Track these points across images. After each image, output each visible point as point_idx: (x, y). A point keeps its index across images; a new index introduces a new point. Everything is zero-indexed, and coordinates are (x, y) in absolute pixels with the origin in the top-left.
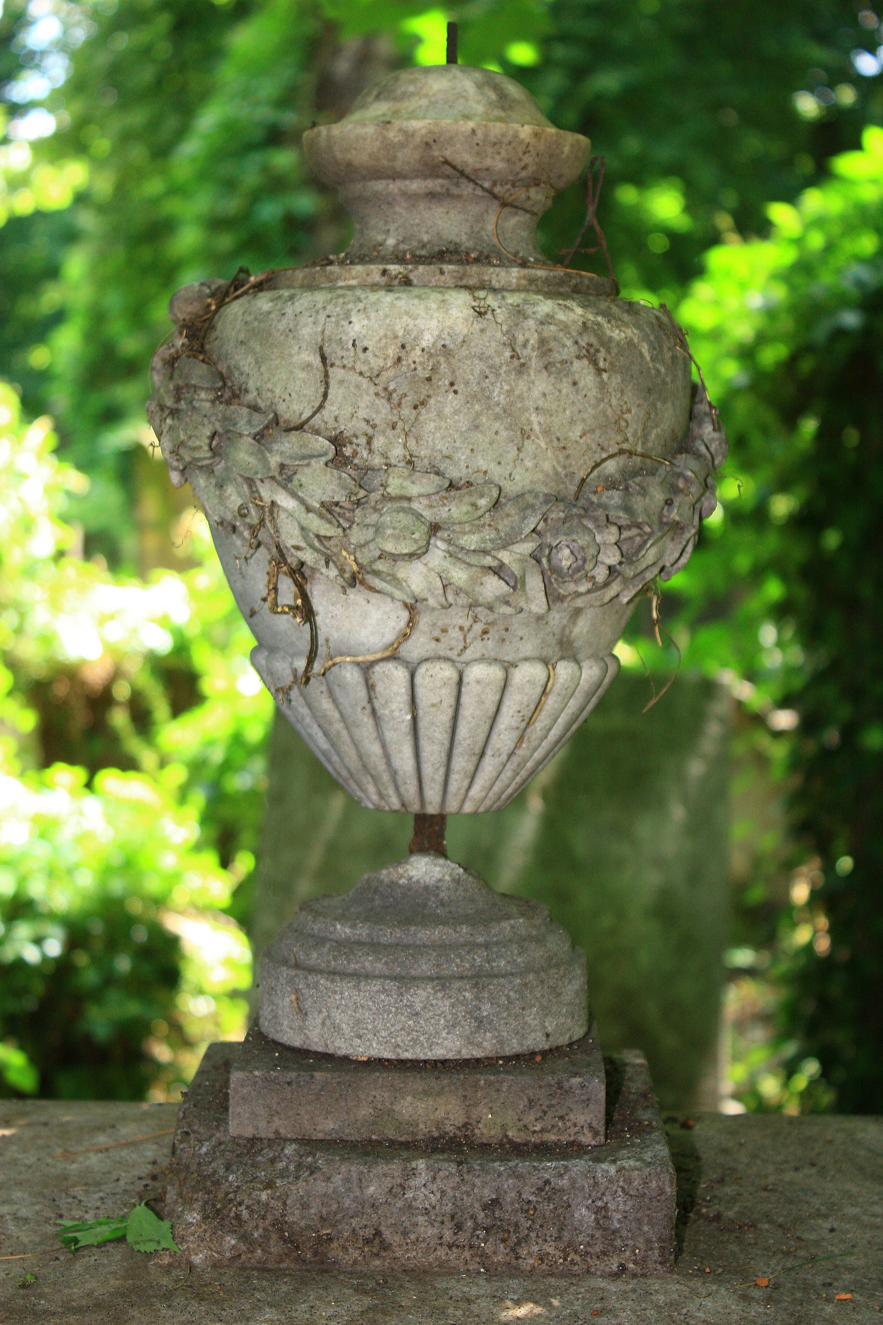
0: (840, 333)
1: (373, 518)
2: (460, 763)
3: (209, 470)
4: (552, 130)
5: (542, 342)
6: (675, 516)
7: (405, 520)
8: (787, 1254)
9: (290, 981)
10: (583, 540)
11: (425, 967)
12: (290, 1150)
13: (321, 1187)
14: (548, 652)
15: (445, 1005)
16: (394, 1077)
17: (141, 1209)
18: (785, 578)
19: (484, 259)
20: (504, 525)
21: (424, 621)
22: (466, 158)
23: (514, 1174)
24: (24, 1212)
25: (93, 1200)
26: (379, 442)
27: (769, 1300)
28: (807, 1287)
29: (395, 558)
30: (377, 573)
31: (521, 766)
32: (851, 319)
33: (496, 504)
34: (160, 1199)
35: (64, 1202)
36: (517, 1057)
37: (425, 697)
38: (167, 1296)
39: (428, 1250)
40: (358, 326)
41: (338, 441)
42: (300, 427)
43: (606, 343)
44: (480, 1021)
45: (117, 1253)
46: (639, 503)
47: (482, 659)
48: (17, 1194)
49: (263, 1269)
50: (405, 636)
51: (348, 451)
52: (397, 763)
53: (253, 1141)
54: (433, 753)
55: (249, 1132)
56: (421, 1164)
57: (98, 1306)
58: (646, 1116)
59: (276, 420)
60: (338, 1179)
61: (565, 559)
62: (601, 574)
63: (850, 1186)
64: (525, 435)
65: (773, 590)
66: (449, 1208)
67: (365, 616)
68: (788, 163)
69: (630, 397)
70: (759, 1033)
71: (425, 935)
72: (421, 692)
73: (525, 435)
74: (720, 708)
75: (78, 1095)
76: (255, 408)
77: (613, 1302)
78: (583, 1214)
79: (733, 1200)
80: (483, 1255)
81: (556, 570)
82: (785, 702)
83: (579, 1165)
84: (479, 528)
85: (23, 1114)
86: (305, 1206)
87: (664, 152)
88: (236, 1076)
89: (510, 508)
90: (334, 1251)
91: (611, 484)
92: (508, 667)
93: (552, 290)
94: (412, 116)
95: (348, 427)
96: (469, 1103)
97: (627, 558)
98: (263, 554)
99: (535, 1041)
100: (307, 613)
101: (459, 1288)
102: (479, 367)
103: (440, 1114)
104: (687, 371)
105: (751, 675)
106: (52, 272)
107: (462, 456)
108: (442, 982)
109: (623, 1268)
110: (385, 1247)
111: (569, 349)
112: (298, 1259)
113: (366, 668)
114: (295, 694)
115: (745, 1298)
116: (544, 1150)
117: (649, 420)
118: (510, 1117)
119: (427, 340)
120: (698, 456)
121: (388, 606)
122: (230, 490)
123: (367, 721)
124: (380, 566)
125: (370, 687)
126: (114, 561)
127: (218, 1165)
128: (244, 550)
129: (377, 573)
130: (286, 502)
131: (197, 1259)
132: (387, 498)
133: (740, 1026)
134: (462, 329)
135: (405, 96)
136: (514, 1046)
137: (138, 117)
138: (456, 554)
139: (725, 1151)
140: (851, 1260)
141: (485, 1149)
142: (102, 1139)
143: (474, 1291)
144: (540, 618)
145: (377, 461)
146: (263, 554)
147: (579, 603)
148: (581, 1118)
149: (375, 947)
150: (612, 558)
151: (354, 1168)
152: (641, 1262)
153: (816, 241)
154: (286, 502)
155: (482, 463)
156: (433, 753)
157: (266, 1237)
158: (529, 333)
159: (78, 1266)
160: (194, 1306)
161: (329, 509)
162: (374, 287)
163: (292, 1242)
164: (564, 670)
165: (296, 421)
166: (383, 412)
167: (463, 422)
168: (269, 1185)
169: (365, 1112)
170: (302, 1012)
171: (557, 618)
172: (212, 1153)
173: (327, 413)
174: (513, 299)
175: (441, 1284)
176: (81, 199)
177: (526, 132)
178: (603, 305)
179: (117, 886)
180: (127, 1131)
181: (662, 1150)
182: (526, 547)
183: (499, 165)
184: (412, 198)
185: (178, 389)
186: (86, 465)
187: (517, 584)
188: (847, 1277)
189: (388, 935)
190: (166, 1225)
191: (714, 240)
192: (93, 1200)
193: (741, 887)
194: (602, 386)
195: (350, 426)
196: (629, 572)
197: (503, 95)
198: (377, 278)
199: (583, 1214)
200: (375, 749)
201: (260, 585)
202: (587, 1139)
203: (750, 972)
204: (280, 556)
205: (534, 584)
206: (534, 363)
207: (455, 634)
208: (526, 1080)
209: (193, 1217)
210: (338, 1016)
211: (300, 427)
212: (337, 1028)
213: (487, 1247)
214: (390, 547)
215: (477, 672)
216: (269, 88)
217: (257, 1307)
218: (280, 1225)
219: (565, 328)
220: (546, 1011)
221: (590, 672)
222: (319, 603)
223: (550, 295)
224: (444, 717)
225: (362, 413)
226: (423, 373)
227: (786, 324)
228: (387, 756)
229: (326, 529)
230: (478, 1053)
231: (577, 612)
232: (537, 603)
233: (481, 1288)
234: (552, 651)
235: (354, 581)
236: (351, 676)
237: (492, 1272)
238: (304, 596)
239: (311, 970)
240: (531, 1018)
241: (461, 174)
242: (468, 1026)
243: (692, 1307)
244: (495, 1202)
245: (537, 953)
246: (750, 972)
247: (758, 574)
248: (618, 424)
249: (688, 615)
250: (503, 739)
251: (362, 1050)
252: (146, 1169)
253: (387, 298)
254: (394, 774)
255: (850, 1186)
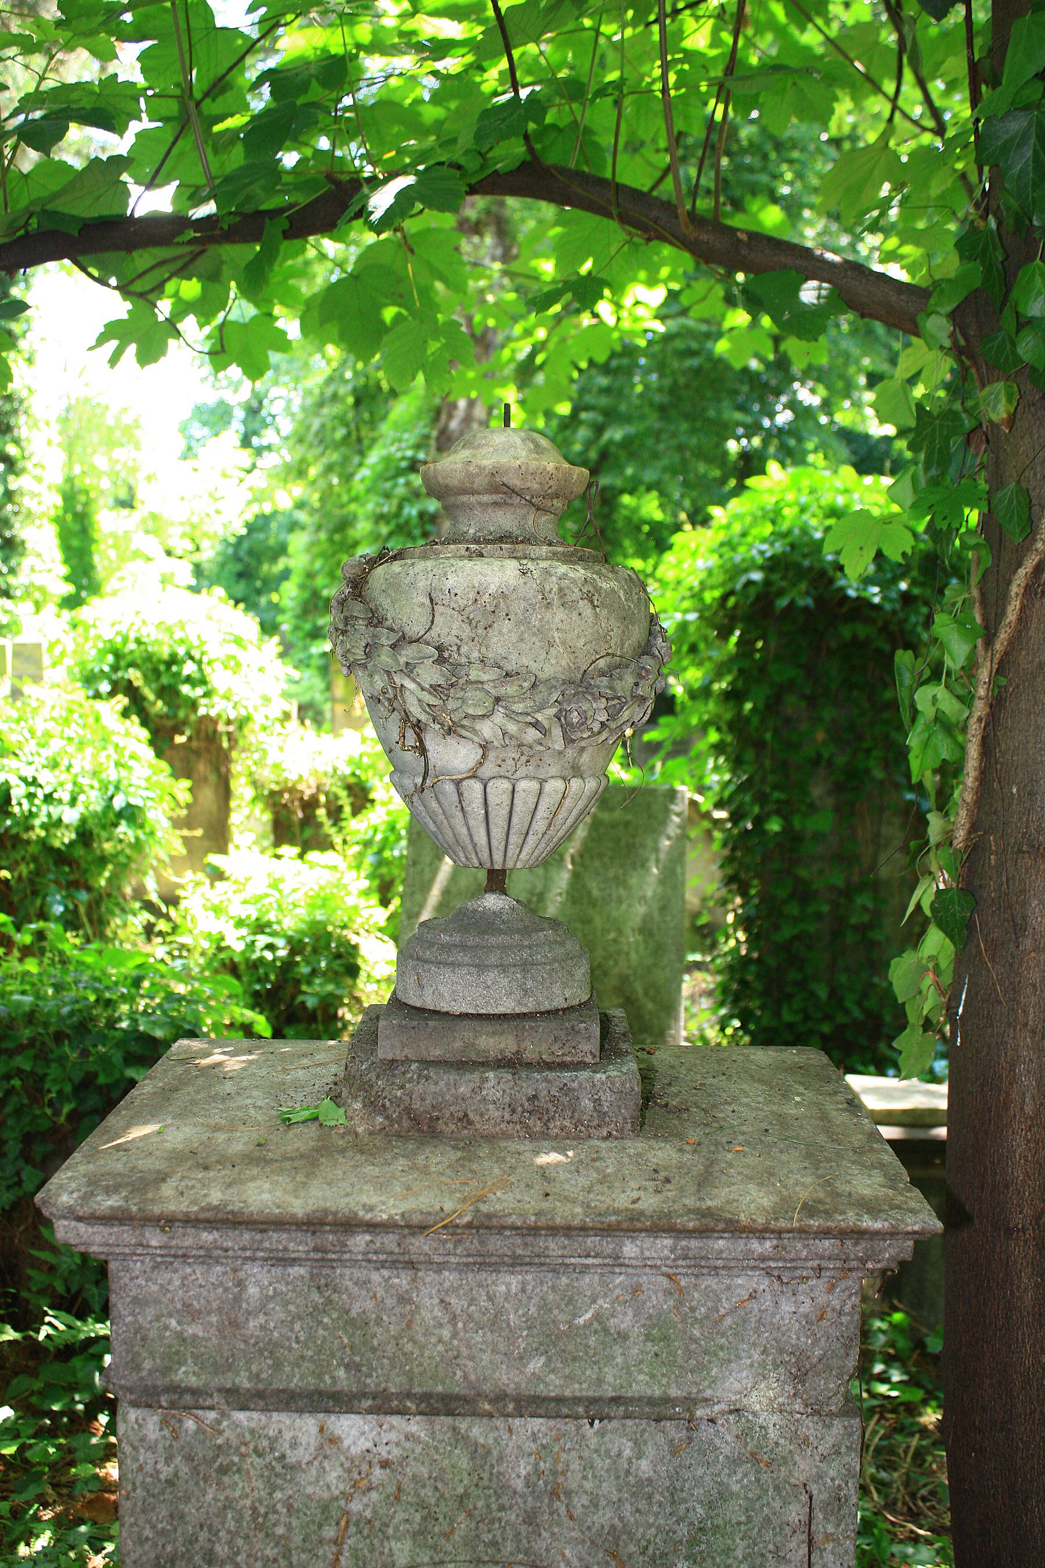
0: (750, 583)
1: (461, 694)
2: (514, 839)
3: (364, 666)
4: (567, 465)
5: (561, 590)
6: (640, 692)
7: (479, 695)
8: (707, 1125)
9: (414, 968)
10: (585, 706)
11: (493, 959)
12: (414, 1066)
13: (432, 1088)
14: (565, 773)
15: (505, 982)
16: (475, 1024)
17: (327, 1101)
18: (719, 729)
19: (526, 541)
20: (538, 698)
21: (492, 755)
22: (516, 482)
23: (546, 1080)
24: (259, 1103)
25: (300, 1096)
26: (464, 649)
27: (695, 1151)
28: (717, 1144)
29: (474, 717)
30: (463, 727)
31: (550, 840)
32: (757, 576)
33: (534, 686)
34: (339, 1096)
35: (282, 1097)
36: (548, 1012)
37: (492, 800)
38: (343, 1151)
39: (496, 1124)
40: (452, 581)
41: (440, 649)
42: (417, 641)
43: (598, 590)
44: (526, 991)
45: (314, 1127)
46: (618, 685)
47: (527, 777)
48: (255, 1093)
49: (398, 1135)
50: (481, 764)
51: (446, 655)
52: (476, 839)
53: (393, 1061)
54: (498, 833)
55: (390, 1057)
56: (491, 1075)
57: (302, 1156)
58: (624, 1046)
59: (404, 637)
60: (442, 1083)
61: (575, 717)
62: (596, 727)
63: (745, 1086)
64: (551, 645)
65: (713, 736)
66: (507, 1100)
67: (457, 752)
68: (723, 481)
69: (614, 623)
70: (705, 1003)
71: (493, 940)
72: (490, 797)
73: (551, 645)
74: (680, 807)
75: (298, 1036)
76: (391, 629)
77: (604, 1154)
78: (587, 1103)
79: (677, 1095)
80: (528, 1127)
81: (570, 724)
82: (719, 805)
83: (584, 1075)
84: (524, 700)
85: (258, 1048)
86: (423, 1099)
87: (650, 475)
88: (382, 1023)
89: (542, 688)
90: (441, 1126)
91: (603, 674)
92: (542, 782)
93: (568, 559)
94: (484, 457)
95: (446, 640)
96: (519, 1039)
97: (612, 717)
98: (396, 715)
99: (559, 1003)
100: (422, 750)
101: (513, 1146)
102: (523, 604)
103: (502, 1046)
104: (647, 607)
105: (701, 789)
106: (282, 550)
107: (513, 657)
108: (503, 968)
109: (610, 1134)
110: (470, 1123)
111: (577, 594)
112: (419, 1130)
113: (458, 783)
114: (415, 798)
115: (681, 1150)
116: (563, 1066)
117: (625, 634)
118: (544, 1047)
119: (492, 589)
120: (653, 656)
121: (470, 746)
122: (376, 677)
123: (459, 814)
124: (465, 722)
125: (460, 794)
126: (318, 721)
127: (373, 1076)
128: (386, 714)
129: (463, 727)
130: (410, 685)
131: (360, 1130)
132: (469, 682)
133: (692, 998)
134: (513, 582)
135: (480, 446)
136: (546, 1006)
137: (335, 456)
138: (510, 715)
139: (673, 1067)
140: (744, 1128)
141: (529, 1065)
142: (305, 1061)
143: (522, 1148)
144: (560, 753)
145: (464, 660)
146: (396, 715)
147: (583, 744)
148: (586, 1047)
149: (464, 947)
150: (603, 717)
151: (452, 1077)
152: (621, 1131)
153: (737, 528)
154: (410, 685)
155: (525, 661)
156: (498, 833)
157: (400, 1117)
158: (552, 584)
159: (291, 1134)
160: (358, 1156)
161: (435, 689)
162: (461, 557)
163: (416, 1120)
164: (575, 784)
165: (415, 637)
166: (467, 631)
167: (514, 637)
168: (402, 1087)
169: (458, 1044)
170: (421, 987)
171: (571, 753)
172: (368, 1069)
173: (433, 633)
174: (544, 564)
175: (503, 1144)
176: (300, 505)
177: (551, 467)
178: (597, 568)
179: (319, 916)
180: (319, 1057)
181: (633, 1066)
182: (553, 711)
183: (536, 486)
184: (485, 506)
185: (346, 618)
186: (299, 664)
187: (545, 732)
188: (741, 1138)
189: (471, 940)
190: (342, 1110)
191: (678, 528)
192: (300, 1096)
193: (697, 915)
194: (596, 616)
195: (448, 640)
196: (613, 725)
197: (537, 445)
198: (463, 552)
199: (587, 1103)
200: (464, 831)
201: (395, 735)
202: (589, 1059)
203: (698, 966)
204: (406, 718)
205: (557, 732)
206: (556, 602)
207: (510, 762)
208: (553, 1025)
209: (358, 1105)
210: (442, 988)
211: (417, 641)
212: (442, 996)
213: (531, 1123)
214: (471, 711)
215: (522, 785)
216: (410, 438)
217: (395, 1157)
218: (408, 1110)
219: (574, 581)
220: (565, 985)
221: (591, 785)
222: (429, 744)
223: (565, 562)
224: (504, 812)
225: (454, 632)
226: (490, 609)
227: (719, 577)
228: (471, 835)
229: (433, 701)
230: (525, 1010)
231: (583, 749)
232: (559, 744)
233: (527, 1146)
234: (568, 773)
235: (450, 731)
236: (449, 788)
237: (532, 1137)
238: (421, 741)
239: (426, 961)
240: (556, 989)
241: (513, 491)
242: (519, 994)
243: (650, 1156)
244: (535, 1097)
245: (560, 951)
246: (698, 966)
247: (704, 728)
248: (605, 638)
249: (662, 753)
250: (540, 825)
251: (457, 1008)
252: (331, 1079)
253: (468, 564)
254: (475, 845)
255: (745, 1086)
